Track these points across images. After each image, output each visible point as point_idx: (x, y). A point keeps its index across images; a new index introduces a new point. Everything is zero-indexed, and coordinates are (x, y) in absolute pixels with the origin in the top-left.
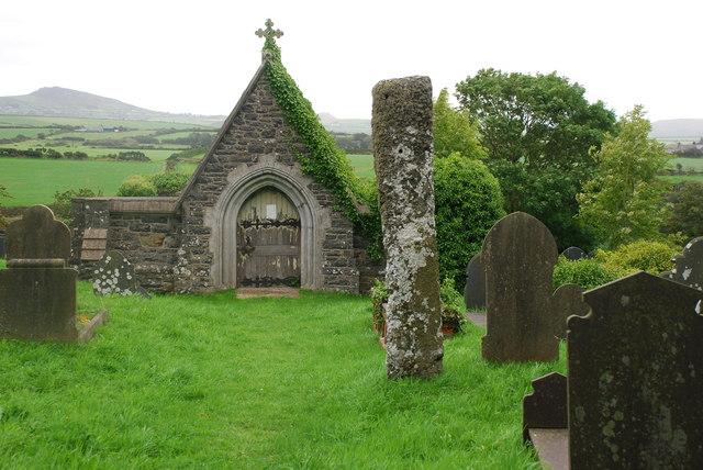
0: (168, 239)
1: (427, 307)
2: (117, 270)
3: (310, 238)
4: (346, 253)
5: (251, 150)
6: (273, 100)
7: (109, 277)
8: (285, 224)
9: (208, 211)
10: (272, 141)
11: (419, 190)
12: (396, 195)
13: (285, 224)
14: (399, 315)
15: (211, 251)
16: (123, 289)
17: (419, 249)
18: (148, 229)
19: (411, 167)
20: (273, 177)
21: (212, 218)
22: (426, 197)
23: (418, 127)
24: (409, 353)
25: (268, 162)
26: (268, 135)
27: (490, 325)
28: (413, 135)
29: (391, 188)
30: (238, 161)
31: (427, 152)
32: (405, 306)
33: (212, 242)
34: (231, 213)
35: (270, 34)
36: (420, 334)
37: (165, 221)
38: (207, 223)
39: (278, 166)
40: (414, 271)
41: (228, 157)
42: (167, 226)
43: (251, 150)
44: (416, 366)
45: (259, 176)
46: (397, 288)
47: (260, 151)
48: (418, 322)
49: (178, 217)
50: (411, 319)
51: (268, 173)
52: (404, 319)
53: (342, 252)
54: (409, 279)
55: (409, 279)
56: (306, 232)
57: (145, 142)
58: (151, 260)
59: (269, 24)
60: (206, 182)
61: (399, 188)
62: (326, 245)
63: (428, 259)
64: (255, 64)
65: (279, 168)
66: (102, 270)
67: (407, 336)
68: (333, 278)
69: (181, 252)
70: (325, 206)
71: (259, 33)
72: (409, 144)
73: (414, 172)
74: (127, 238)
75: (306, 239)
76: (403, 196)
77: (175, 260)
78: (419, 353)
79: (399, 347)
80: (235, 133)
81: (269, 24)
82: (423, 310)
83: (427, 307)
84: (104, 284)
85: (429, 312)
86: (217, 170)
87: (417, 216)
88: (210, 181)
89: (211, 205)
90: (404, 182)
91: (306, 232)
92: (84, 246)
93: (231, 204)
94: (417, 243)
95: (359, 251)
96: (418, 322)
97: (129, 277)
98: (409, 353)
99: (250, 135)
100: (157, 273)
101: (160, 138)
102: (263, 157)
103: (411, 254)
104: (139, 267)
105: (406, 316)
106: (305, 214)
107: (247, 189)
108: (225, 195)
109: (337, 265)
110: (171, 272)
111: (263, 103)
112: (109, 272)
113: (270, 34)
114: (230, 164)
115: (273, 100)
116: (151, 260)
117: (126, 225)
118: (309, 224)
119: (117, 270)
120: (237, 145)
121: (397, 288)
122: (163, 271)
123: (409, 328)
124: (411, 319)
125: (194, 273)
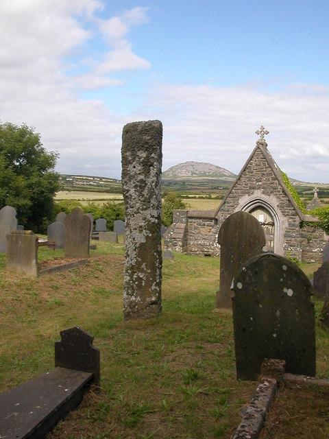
8: (267, 224)
10: (260, 183)
11: (145, 192)
13: (267, 224)
17: (142, 231)
19: (142, 177)
25: (258, 194)
26: (258, 181)
29: (128, 191)
30: (244, 193)
36: (139, 286)
40: (138, 245)
42: (213, 223)
43: (251, 188)
44: (137, 307)
45: (108, 179)
47: (254, 188)
52: (131, 276)
53: (293, 239)
55: (135, 250)
57: (307, 190)
61: (132, 191)
62: (285, 236)
63: (147, 237)
65: (264, 197)
67: (132, 287)
71: (257, 133)
73: (142, 181)
74: (195, 228)
76: (134, 196)
78: (139, 298)
79: (128, 294)
82: (142, 271)
85: (145, 272)
87: (143, 209)
94: (141, 227)
95: (303, 239)
96: (139, 279)
101: (304, 193)
102: (256, 191)
103: (136, 234)
105: (133, 273)
109: (291, 246)
123: (134, 282)
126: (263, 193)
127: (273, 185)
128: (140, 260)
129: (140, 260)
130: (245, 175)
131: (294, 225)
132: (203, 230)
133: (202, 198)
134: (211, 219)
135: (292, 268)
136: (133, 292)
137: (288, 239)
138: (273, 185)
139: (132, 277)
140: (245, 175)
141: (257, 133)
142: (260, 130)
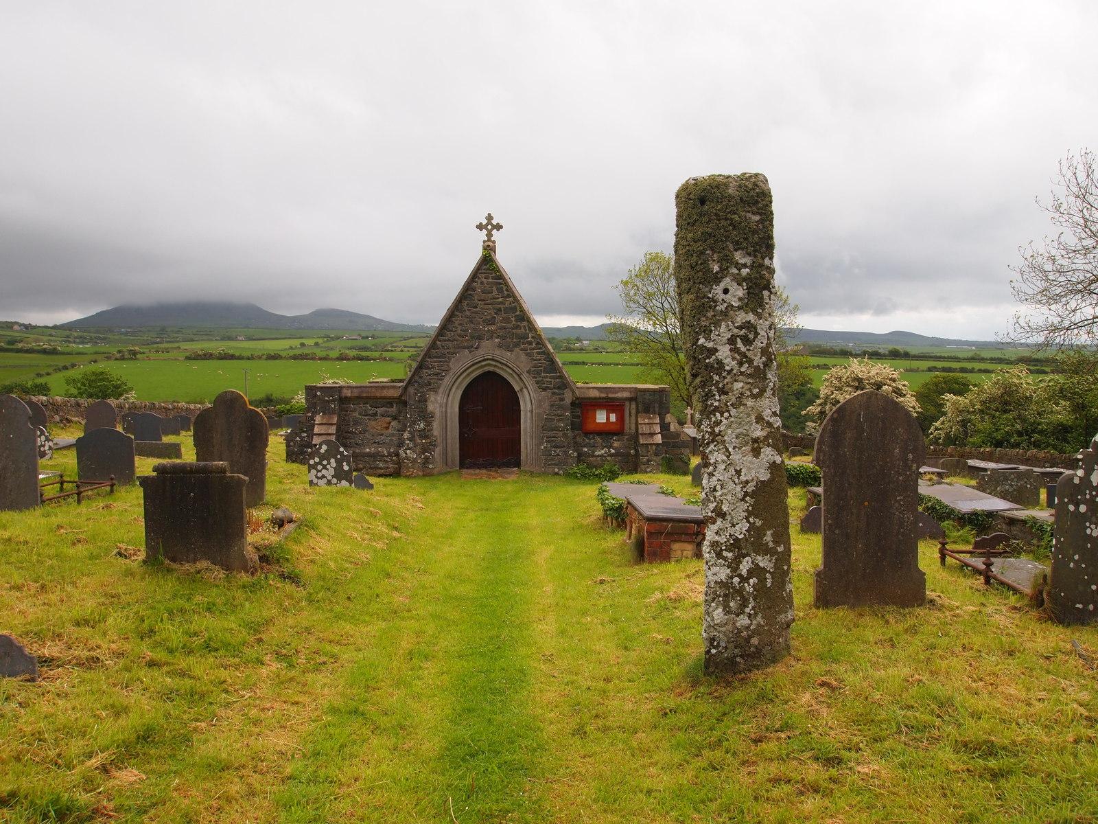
0: (394, 423)
1: (771, 545)
2: (333, 461)
3: (529, 421)
4: (565, 435)
5: (472, 337)
6: (488, 294)
7: (325, 467)
9: (432, 397)
10: (493, 327)
12: (720, 362)
14: (725, 559)
15: (435, 434)
16: (340, 479)
18: (376, 414)
19: (741, 317)
20: (494, 363)
21: (435, 403)
22: (766, 365)
23: (753, 254)
24: (743, 621)
26: (492, 322)
27: (827, 555)
28: (745, 266)
31: (766, 293)
32: (736, 544)
33: (435, 425)
34: (457, 388)
35: (490, 226)
36: (760, 589)
37: (392, 406)
38: (430, 408)
39: (498, 352)
40: (750, 488)
41: (450, 344)
42: (393, 410)
43: (472, 337)
45: (480, 362)
46: (722, 515)
47: (480, 338)
48: (756, 571)
49: (402, 402)
50: (745, 566)
51: (488, 359)
52: (734, 566)
53: (561, 434)
54: (743, 499)
55: (743, 499)
56: (526, 415)
58: (378, 443)
59: (490, 218)
60: (429, 368)
61: (724, 352)
62: (544, 428)
64: (478, 254)
66: (317, 460)
67: (740, 592)
68: (552, 459)
69: (406, 435)
70: (544, 389)
72: (739, 281)
73: (748, 326)
75: (525, 421)
76: (730, 364)
77: (401, 444)
80: (456, 321)
81: (490, 218)
82: (765, 551)
83: (771, 545)
84: (320, 475)
86: (439, 357)
88: (433, 368)
89: (435, 390)
90: (732, 341)
91: (526, 415)
92: (316, 430)
93: (454, 389)
94: (756, 440)
96: (756, 571)
97: (346, 468)
98: (743, 621)
99: (471, 322)
100: (384, 456)
102: (485, 343)
104: (368, 450)
105: (737, 560)
106: (525, 400)
107: (468, 375)
108: (447, 381)
110: (398, 455)
111: (483, 292)
112: (325, 462)
113: (490, 226)
114: (452, 350)
115: (488, 294)
116: (378, 443)
117: (355, 410)
118: (529, 408)
119: (333, 461)
120: (459, 332)
121: (722, 515)
122: (390, 454)
123: (744, 580)
124: (745, 566)
125: (419, 455)
126: (500, 346)
127: (519, 331)
128: (759, 523)
129: (759, 523)
130: (462, 311)
131: (561, 407)
132: (375, 425)
133: (207, 356)
134: (389, 402)
135: (432, 475)
136: (744, 604)
137: (551, 433)
138: (519, 331)
139: (735, 570)
140: (462, 311)
141: (480, 227)
142: (485, 222)
